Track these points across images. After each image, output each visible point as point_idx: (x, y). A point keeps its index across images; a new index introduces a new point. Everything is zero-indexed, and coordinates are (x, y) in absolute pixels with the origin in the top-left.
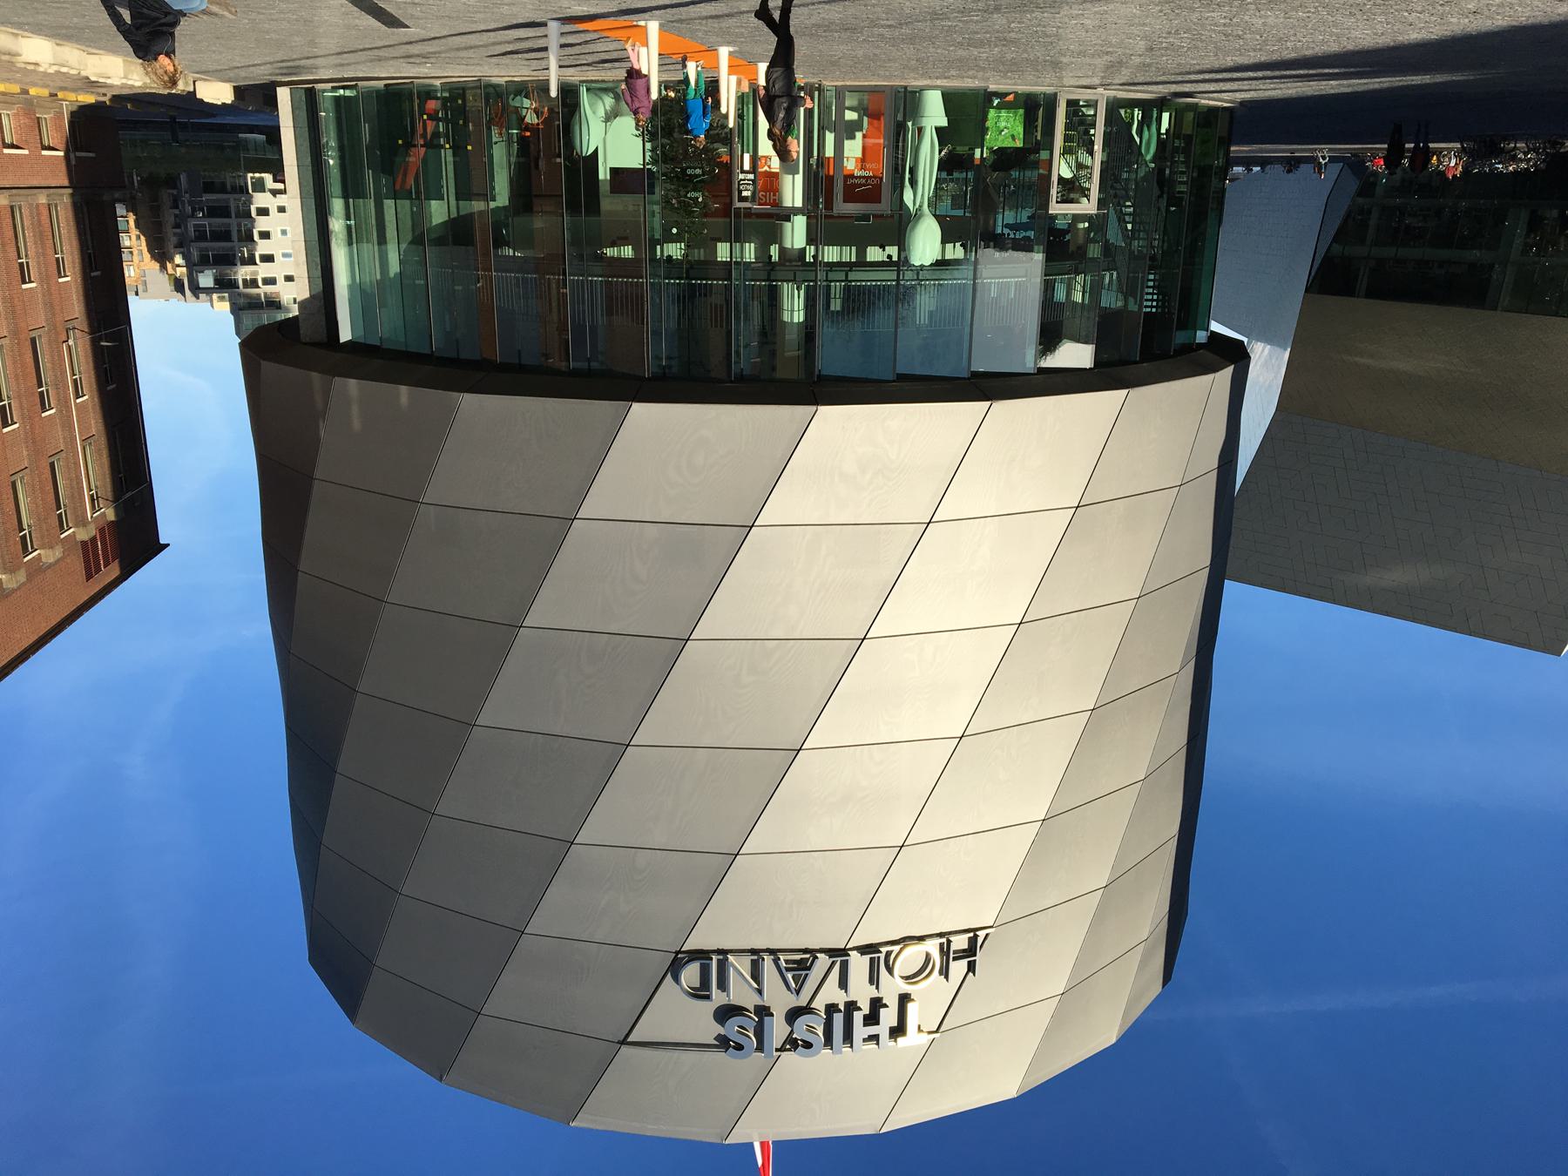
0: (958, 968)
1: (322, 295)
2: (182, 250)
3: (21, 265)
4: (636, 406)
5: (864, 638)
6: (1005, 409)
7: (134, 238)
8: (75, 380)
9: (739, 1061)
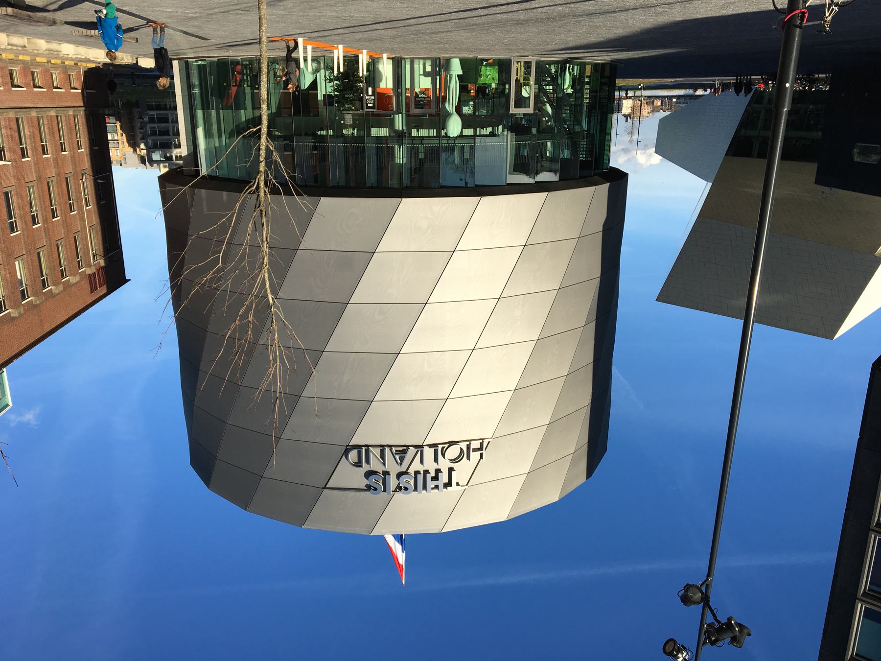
0: (475, 456)
1: (193, 153)
2: (144, 141)
3: (61, 143)
4: (322, 199)
5: (426, 303)
6: (487, 200)
7: (119, 135)
8: (86, 198)
9: (375, 496)
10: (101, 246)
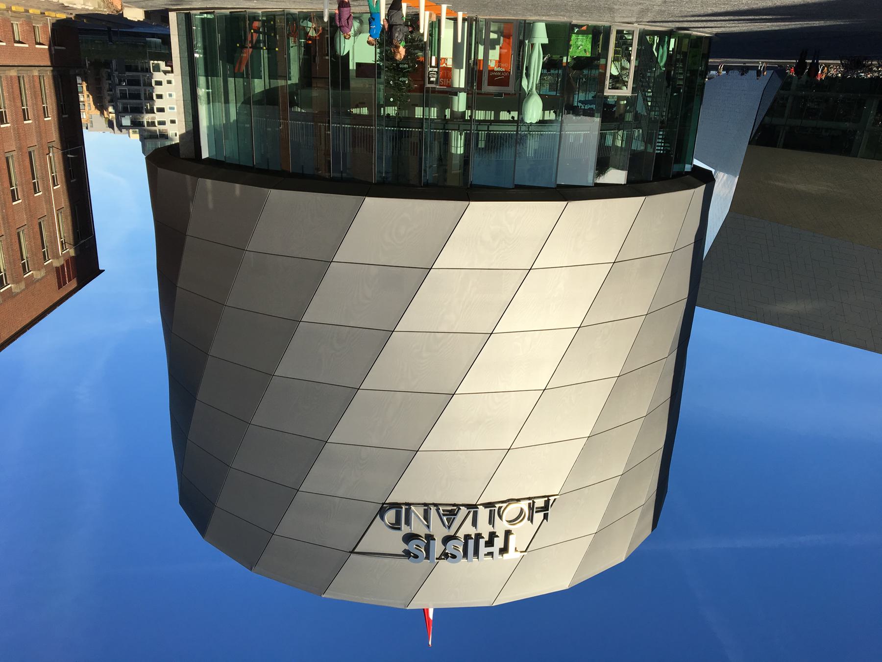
0: (539, 517)
1: (192, 131)
2: (113, 104)
3: (24, 110)
6: (575, 206)
7: (86, 96)
8: (53, 177)
10: (71, 233)
